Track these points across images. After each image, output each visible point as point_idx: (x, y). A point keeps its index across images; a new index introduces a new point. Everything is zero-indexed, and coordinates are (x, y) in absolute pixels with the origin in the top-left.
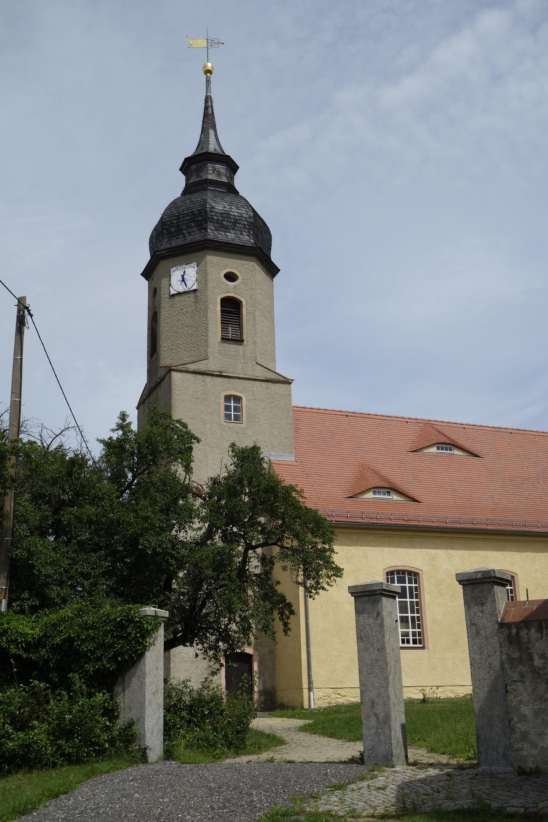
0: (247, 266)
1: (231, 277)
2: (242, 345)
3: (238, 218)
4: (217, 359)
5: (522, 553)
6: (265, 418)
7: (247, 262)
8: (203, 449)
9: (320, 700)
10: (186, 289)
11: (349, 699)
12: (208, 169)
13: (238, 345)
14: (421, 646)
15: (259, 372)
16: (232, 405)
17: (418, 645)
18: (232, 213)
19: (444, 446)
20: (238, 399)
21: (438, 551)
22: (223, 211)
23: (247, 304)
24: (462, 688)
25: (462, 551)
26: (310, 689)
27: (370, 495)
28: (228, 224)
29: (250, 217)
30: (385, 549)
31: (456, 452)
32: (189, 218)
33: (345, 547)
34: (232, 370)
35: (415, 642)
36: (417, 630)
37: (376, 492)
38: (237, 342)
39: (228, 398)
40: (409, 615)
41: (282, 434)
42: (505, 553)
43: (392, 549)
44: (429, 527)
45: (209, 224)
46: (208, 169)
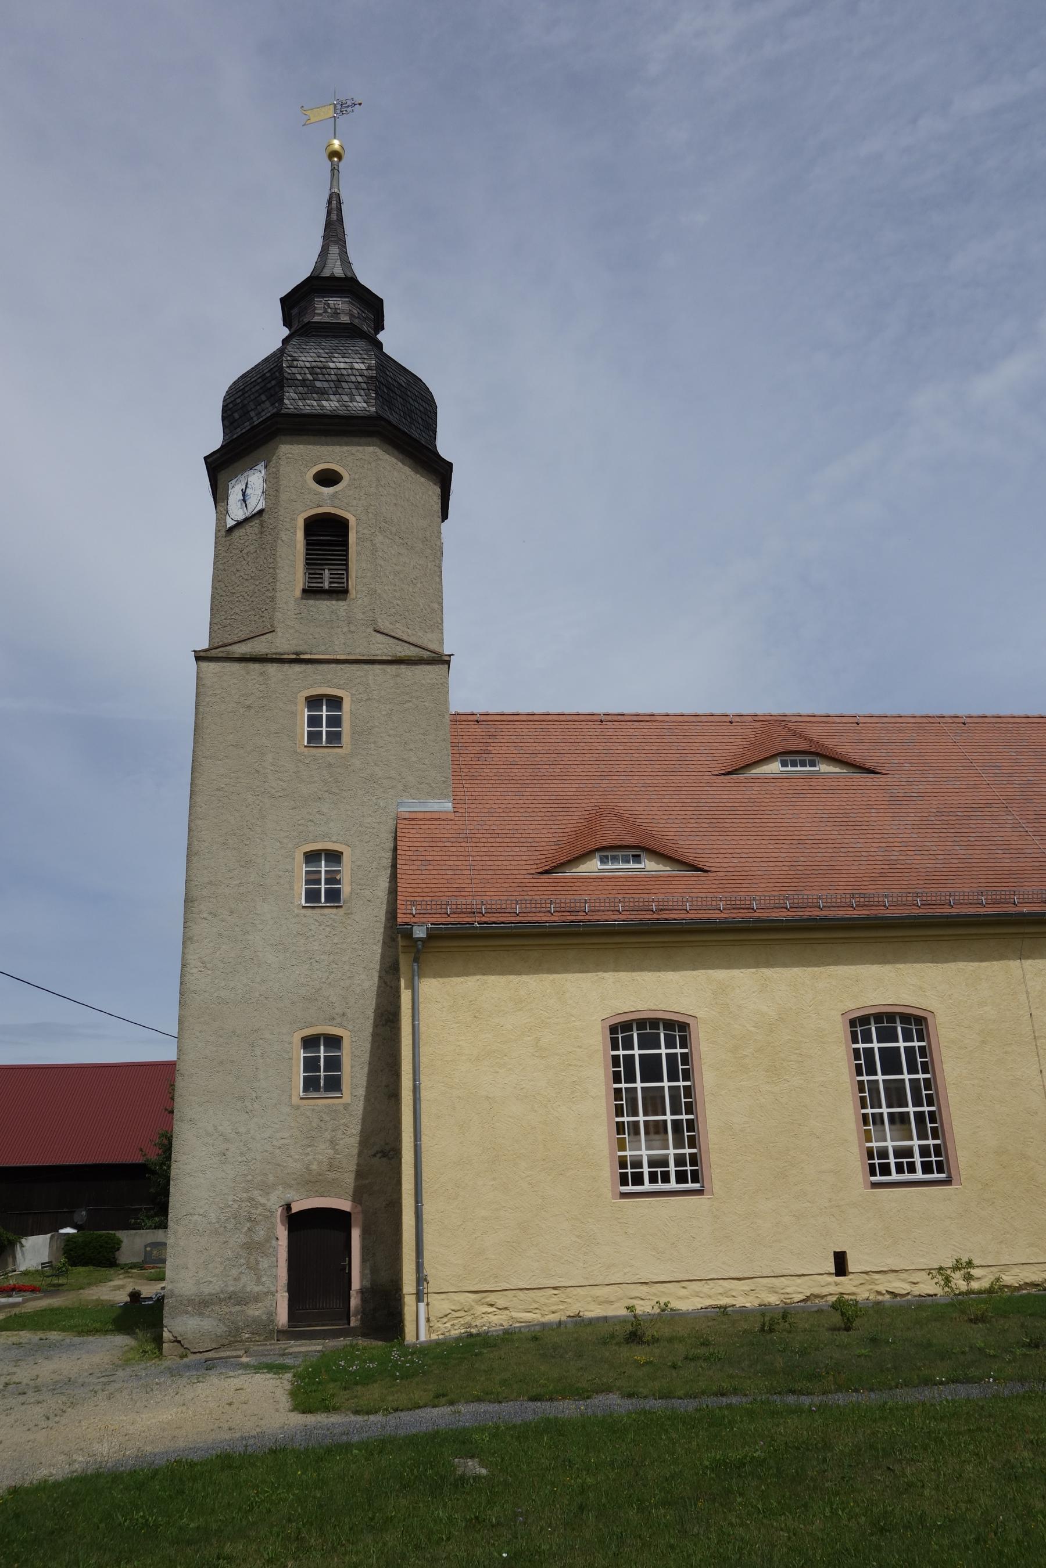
0: (360, 456)
1: (328, 478)
2: (345, 600)
3: (344, 372)
4: (292, 631)
5: (945, 965)
6: (391, 732)
7: (360, 448)
8: (257, 802)
9: (445, 1320)
10: (248, 514)
11: (515, 1314)
12: (331, 306)
13: (337, 600)
14: (942, 1176)
15: (381, 646)
16: (324, 713)
17: (936, 1176)
18: (332, 365)
19: (798, 758)
20: (335, 702)
21: (735, 972)
22: (314, 364)
23: (358, 524)
24: (799, 1281)
25: (795, 969)
26: (419, 1296)
27: (593, 866)
28: (326, 384)
29: (369, 368)
30: (606, 975)
31: (824, 768)
32: (258, 387)
33: (511, 977)
34: (323, 648)
35: (927, 1168)
36: (931, 1142)
37: (607, 857)
38: (334, 595)
39: (314, 702)
40: (911, 1109)
41: (426, 762)
42: (901, 966)
43: (624, 976)
44: (709, 922)
45: (286, 389)
46: (331, 306)
